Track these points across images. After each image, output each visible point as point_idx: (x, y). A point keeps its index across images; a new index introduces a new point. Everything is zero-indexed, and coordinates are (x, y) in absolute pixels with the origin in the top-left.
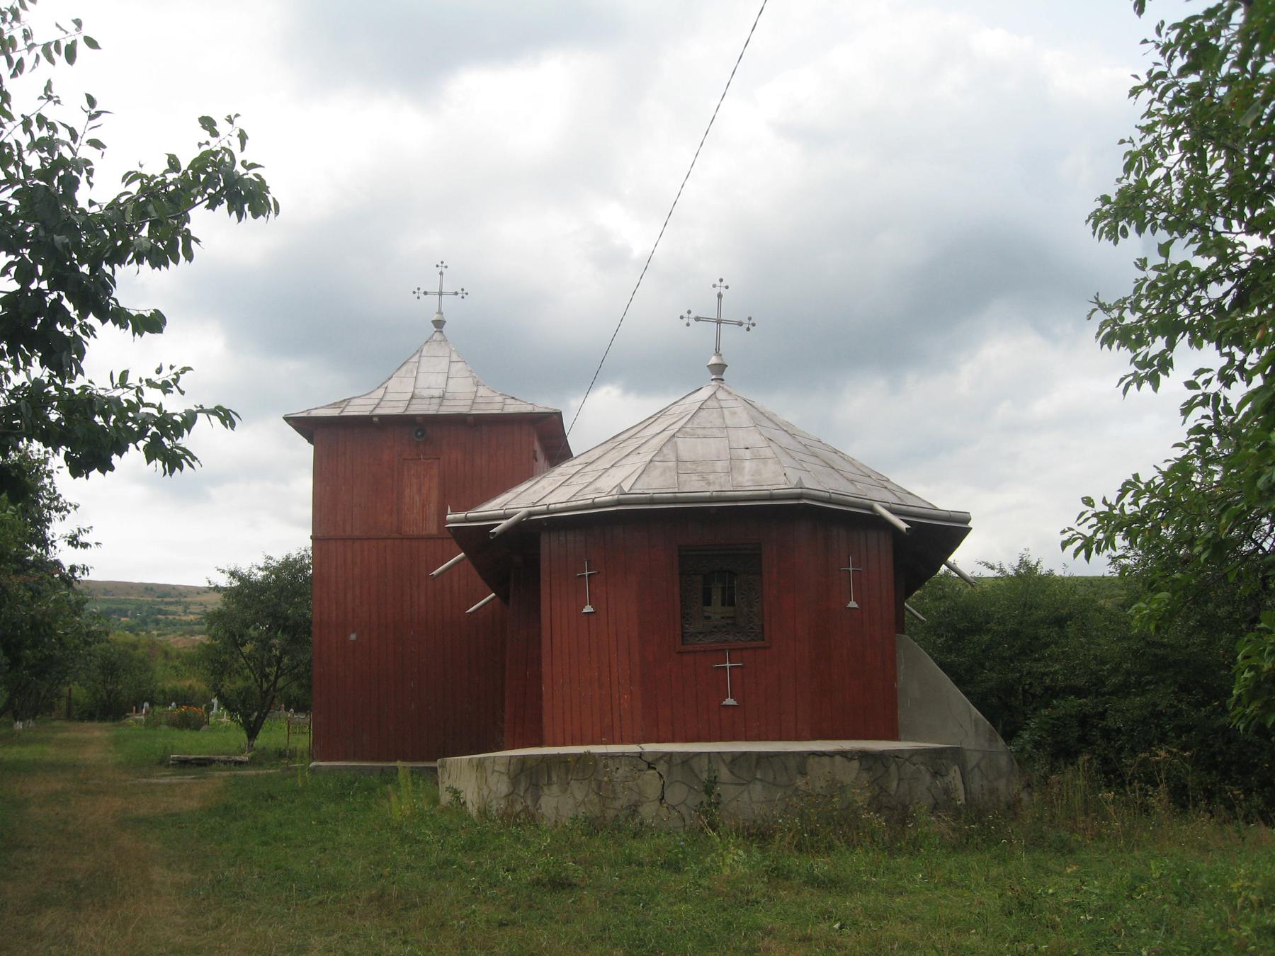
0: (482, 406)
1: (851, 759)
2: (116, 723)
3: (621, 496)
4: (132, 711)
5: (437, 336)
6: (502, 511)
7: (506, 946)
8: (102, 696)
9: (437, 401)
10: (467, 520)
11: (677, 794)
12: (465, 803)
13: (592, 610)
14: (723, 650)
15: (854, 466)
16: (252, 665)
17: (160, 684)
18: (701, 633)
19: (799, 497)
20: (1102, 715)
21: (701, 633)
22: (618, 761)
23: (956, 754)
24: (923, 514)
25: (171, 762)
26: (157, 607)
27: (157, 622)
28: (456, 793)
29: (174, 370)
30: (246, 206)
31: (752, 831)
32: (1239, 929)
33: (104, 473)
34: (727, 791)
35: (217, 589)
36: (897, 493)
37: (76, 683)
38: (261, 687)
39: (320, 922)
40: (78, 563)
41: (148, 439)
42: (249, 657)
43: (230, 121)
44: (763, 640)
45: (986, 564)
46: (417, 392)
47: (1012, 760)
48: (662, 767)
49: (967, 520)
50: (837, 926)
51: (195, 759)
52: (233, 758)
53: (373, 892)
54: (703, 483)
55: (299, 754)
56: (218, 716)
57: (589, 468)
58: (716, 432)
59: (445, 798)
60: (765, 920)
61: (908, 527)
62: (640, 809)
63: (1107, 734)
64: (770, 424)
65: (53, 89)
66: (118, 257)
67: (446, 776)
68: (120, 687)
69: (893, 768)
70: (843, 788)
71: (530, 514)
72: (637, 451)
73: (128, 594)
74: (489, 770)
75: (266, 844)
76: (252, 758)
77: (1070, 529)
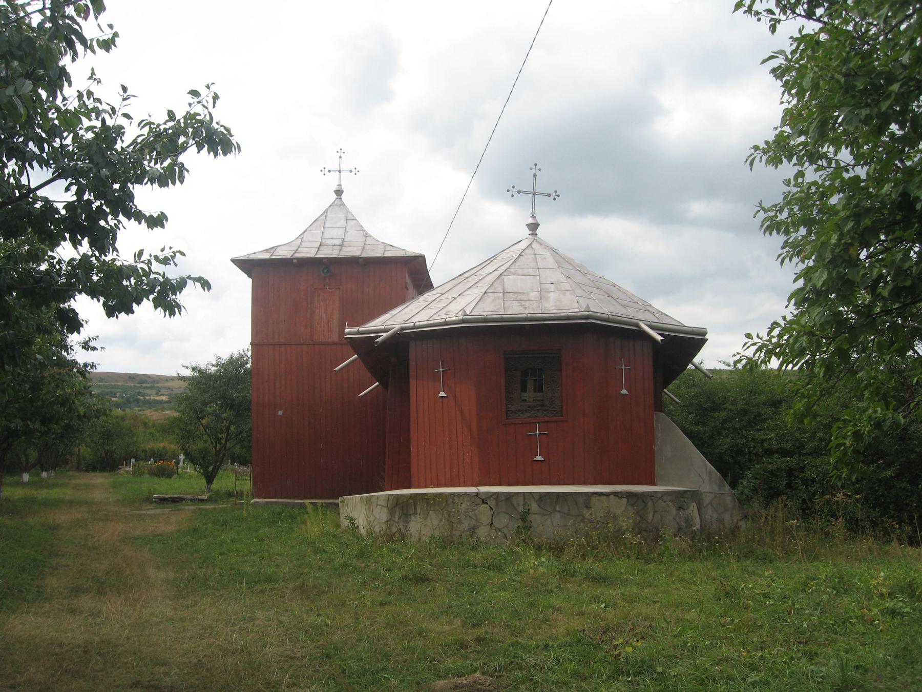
0: (370, 252)
1: (621, 498)
2: (112, 473)
3: (464, 317)
4: (123, 464)
5: (338, 201)
6: (383, 327)
7: (384, 617)
8: (101, 454)
9: (338, 248)
10: (359, 333)
11: (502, 521)
12: (358, 526)
13: (444, 395)
14: (535, 423)
15: (627, 295)
16: (209, 432)
17: (142, 446)
18: (519, 411)
19: (587, 317)
20: (802, 469)
21: (519, 411)
22: (462, 498)
23: (695, 495)
24: (675, 329)
25: (154, 500)
26: (138, 390)
27: (138, 401)
28: (352, 520)
29: (172, 250)
30: (219, 148)
31: (552, 546)
32: (870, 610)
33: (128, 315)
34: (536, 520)
35: (182, 378)
36: (656, 315)
37: (84, 445)
38: (215, 447)
39: (262, 603)
40: (89, 361)
41: (156, 294)
42: (206, 427)
43: (208, 87)
44: (562, 416)
45: (724, 363)
46: (323, 241)
47: (734, 499)
48: (492, 502)
49: (705, 334)
50: (603, 606)
51: (171, 498)
52: (197, 497)
53: (297, 584)
54: (521, 308)
55: (245, 493)
56: (184, 468)
57: (443, 297)
58: (531, 272)
59: (345, 523)
60: (553, 601)
61: (662, 338)
62: (477, 531)
63: (805, 482)
64: (571, 267)
65: (96, 73)
66: (139, 180)
67: (345, 509)
68: (114, 448)
69: (650, 504)
70: (615, 517)
71: (402, 329)
72: (477, 285)
73: (116, 381)
74: (374, 505)
75: (222, 554)
76: (210, 497)
77: (739, 354)
